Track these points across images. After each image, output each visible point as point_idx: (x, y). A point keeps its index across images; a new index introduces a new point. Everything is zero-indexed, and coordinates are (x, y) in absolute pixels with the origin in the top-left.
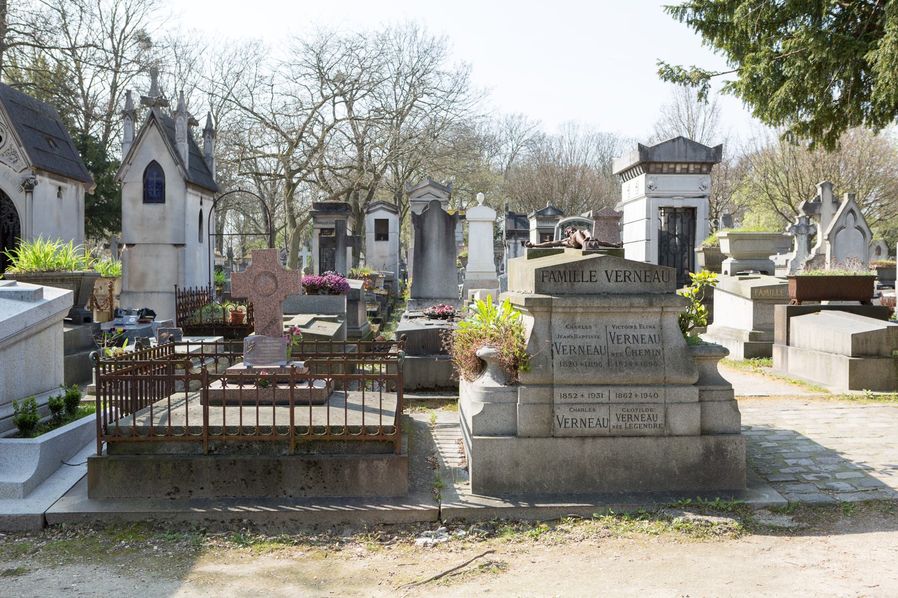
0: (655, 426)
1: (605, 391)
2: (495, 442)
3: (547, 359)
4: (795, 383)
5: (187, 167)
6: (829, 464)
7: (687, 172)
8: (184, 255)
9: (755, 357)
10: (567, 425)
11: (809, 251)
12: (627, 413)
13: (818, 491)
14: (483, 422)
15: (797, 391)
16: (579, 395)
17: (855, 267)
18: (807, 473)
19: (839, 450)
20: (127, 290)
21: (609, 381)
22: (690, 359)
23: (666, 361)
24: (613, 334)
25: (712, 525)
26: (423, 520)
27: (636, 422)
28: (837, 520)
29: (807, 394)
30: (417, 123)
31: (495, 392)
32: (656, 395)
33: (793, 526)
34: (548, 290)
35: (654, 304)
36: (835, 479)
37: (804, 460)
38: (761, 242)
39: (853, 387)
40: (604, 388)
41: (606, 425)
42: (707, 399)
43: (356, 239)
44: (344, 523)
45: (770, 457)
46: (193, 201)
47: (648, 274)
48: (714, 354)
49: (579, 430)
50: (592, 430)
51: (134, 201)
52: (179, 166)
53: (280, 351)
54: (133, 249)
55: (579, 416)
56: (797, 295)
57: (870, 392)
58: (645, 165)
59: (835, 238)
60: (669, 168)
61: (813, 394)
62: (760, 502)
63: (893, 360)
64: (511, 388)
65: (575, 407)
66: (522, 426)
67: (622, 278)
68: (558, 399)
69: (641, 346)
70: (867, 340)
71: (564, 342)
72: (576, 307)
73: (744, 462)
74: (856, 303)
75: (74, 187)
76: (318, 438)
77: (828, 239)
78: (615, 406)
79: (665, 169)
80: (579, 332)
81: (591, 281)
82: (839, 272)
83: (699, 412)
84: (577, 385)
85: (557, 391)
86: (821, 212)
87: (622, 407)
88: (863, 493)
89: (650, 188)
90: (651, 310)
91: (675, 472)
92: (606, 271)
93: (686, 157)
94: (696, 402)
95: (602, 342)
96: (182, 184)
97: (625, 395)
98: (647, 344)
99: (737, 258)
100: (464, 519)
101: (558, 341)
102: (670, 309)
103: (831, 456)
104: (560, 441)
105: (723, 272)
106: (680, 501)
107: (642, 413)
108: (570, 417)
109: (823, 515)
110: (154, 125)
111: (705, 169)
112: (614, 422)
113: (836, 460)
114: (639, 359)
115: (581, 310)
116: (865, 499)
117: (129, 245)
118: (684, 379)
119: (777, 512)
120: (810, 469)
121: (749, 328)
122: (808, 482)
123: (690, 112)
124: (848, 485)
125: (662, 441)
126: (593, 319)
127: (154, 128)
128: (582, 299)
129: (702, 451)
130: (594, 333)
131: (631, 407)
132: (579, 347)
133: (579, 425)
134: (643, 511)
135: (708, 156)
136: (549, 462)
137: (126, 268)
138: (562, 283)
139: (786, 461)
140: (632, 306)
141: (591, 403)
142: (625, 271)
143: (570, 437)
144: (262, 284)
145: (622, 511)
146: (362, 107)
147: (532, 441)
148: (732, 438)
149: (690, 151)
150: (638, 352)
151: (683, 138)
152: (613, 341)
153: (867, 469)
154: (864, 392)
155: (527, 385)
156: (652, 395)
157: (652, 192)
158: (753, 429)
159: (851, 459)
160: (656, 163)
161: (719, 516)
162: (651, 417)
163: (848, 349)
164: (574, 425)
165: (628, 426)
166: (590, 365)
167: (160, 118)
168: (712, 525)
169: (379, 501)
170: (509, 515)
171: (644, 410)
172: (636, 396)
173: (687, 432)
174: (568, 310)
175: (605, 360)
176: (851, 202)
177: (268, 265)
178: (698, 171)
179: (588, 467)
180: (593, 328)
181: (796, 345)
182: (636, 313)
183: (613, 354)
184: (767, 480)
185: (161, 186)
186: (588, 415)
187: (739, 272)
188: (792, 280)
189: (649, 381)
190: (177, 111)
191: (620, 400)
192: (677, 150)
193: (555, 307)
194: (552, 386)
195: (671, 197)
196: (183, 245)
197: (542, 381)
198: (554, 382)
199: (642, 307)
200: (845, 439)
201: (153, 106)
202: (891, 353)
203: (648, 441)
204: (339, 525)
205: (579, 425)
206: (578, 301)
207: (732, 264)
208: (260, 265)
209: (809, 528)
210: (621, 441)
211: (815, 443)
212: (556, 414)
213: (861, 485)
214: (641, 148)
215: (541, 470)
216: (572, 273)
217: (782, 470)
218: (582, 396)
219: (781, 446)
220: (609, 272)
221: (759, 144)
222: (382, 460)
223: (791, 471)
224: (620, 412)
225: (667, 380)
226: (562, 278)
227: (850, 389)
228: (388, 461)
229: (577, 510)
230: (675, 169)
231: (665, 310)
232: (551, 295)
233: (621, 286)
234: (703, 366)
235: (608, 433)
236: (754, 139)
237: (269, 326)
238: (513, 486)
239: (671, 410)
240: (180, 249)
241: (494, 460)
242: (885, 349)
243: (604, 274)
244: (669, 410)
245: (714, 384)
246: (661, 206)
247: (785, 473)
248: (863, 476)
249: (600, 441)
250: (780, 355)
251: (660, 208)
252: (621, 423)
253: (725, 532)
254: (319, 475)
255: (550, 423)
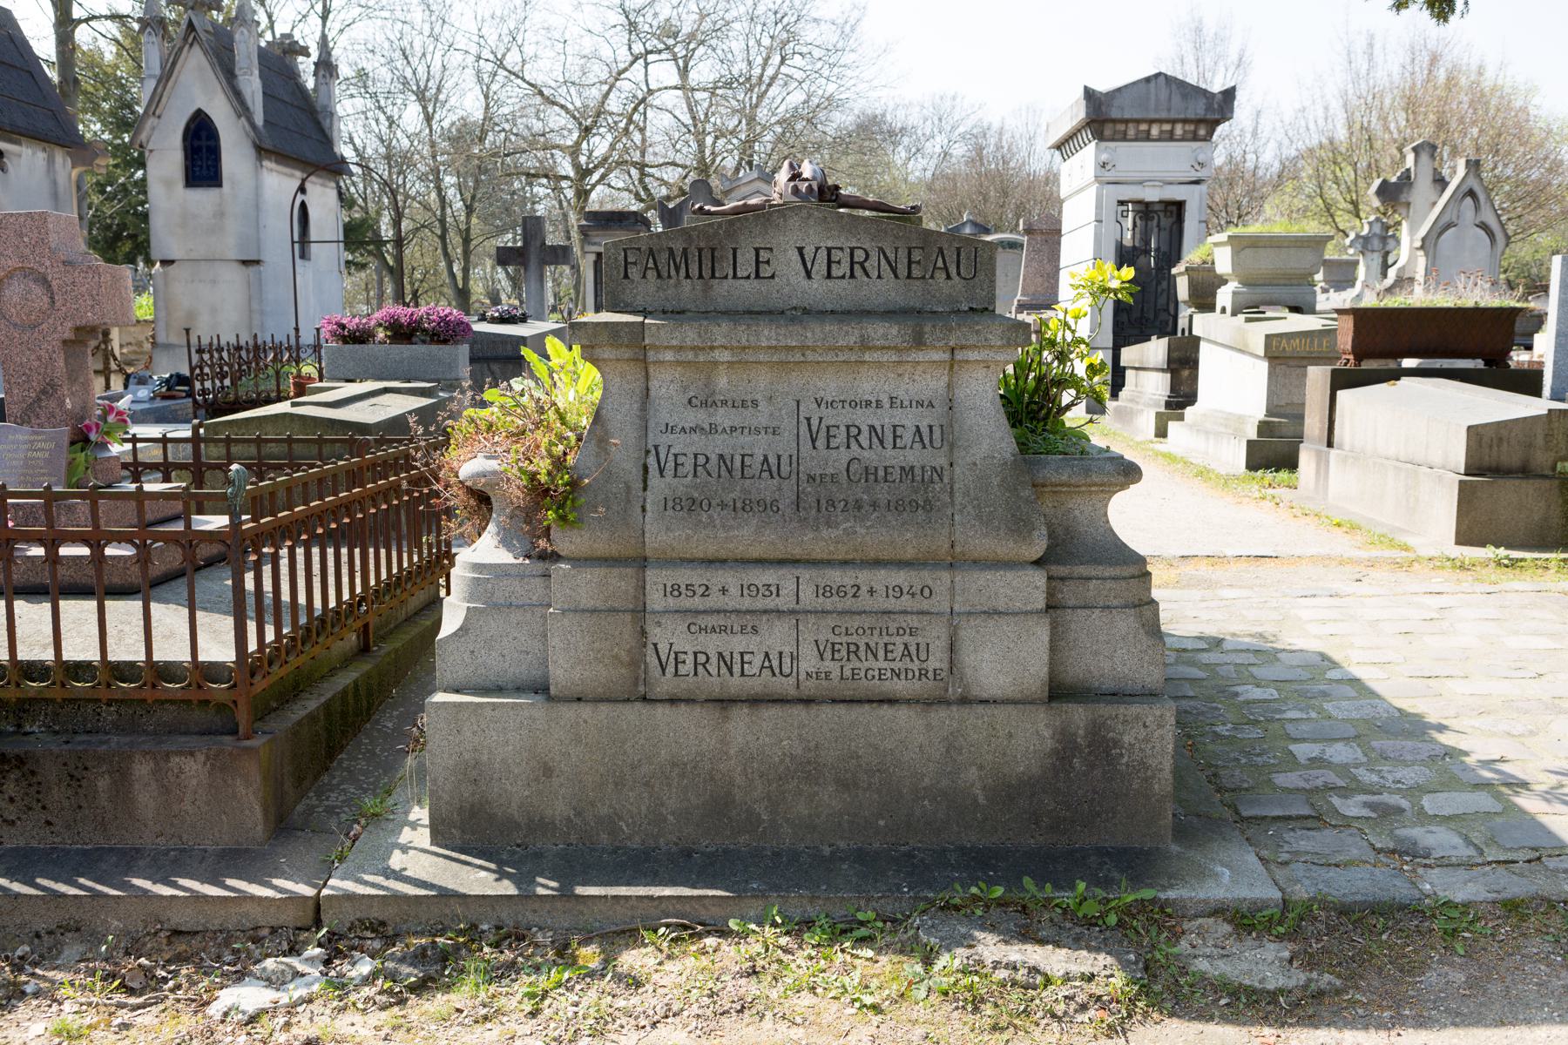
0: (923, 673)
1: (784, 579)
2: (488, 713)
3: (628, 489)
4: (1339, 525)
5: (259, 119)
6: (1405, 764)
7: (1171, 137)
8: (260, 280)
9: (1267, 467)
10: (683, 669)
11: (1385, 275)
12: (844, 639)
13: (1371, 856)
14: (466, 656)
15: (1342, 545)
16: (714, 589)
17: (1477, 291)
18: (1345, 792)
19: (1432, 718)
20: (165, 341)
21: (797, 552)
22: (1026, 492)
23: (958, 498)
24: (815, 422)
25: (1048, 981)
26: (274, 923)
27: (871, 663)
28: (1423, 967)
29: (1364, 554)
30: (784, 100)
31: (497, 577)
32: (927, 591)
33: (1291, 983)
34: (640, 302)
35: (928, 338)
36: (1423, 817)
37: (1339, 746)
38: (1292, 251)
39: (1463, 538)
40: (783, 571)
41: (786, 670)
42: (1071, 603)
43: (560, 252)
44: (65, 929)
45: (1255, 733)
46: (279, 183)
47: (916, 256)
48: (1095, 478)
49: (715, 681)
50: (749, 682)
51: (168, 184)
52: (243, 119)
53: (48, 461)
54: (171, 268)
55: (713, 644)
56: (1353, 347)
57: (1502, 552)
58: (1096, 125)
59: (1435, 245)
60: (1138, 131)
61: (1375, 553)
62: (1202, 895)
63: (1557, 482)
64: (540, 566)
65: (704, 621)
66: (561, 674)
67: (845, 268)
68: (656, 600)
69: (891, 457)
70: (1501, 439)
71: (679, 443)
72: (712, 348)
73: (1167, 774)
74: (1479, 364)
75: (41, 156)
76: (31, 694)
77: (1422, 247)
78: (812, 619)
79: (1131, 132)
80: (724, 417)
81: (758, 276)
82: (1443, 300)
83: (1046, 639)
84: (710, 562)
85: (656, 579)
86: (1411, 200)
87: (831, 621)
88: (1501, 869)
89: (1103, 167)
90: (920, 356)
91: (975, 800)
92: (800, 250)
93: (1169, 110)
94: (1038, 612)
95: (784, 445)
96: (250, 152)
97: (840, 591)
98: (908, 452)
99: (1244, 283)
100: (383, 924)
101: (664, 440)
102: (973, 355)
103: (1409, 735)
104: (661, 711)
105: (1218, 308)
106: (974, 890)
107: (886, 639)
108: (690, 649)
109: (1381, 945)
110: (196, 44)
111: (1202, 132)
112: (809, 663)
113: (1425, 750)
114: (882, 493)
115: (725, 356)
116: (1506, 895)
117: (166, 263)
118: (1006, 547)
119: (1250, 928)
120: (1354, 779)
121: (1260, 413)
122: (1346, 823)
123: (1201, 69)
124: (1457, 841)
125: (940, 715)
126: (762, 380)
127: (196, 49)
128: (725, 326)
129: (1050, 744)
130: (763, 420)
131: (855, 622)
132: (721, 456)
133: (713, 669)
134: (871, 915)
135: (1209, 108)
136: (633, 767)
137: (161, 304)
138: (678, 284)
139: (1292, 747)
140: (865, 345)
141: (748, 612)
142: (852, 250)
143: (690, 701)
144: (16, 299)
145: (811, 911)
146: (704, 71)
147: (586, 711)
148: (1135, 709)
149: (1176, 99)
150: (881, 473)
151: (1166, 75)
152: (813, 441)
153: (1508, 785)
154: (1489, 552)
155: (579, 561)
156: (915, 589)
157: (1107, 174)
158: (1226, 646)
159: (1463, 746)
160: (1114, 121)
161: (1077, 943)
162: (913, 649)
163: (1459, 458)
164: (700, 668)
165: (848, 673)
166: (746, 506)
167: (207, 31)
168: (1048, 981)
169: (167, 866)
170: (504, 915)
171: (892, 630)
172: (871, 591)
173: (1010, 692)
174: (690, 356)
175: (789, 495)
176: (1471, 175)
177: (27, 251)
178: (1190, 136)
179: (739, 780)
180: (762, 405)
181: (1347, 447)
182: (880, 364)
183: (811, 478)
184: (1237, 812)
185: (214, 152)
186: (737, 643)
187: (1250, 307)
188: (1345, 317)
189: (910, 553)
190: (236, 18)
191: (828, 604)
192: (1153, 97)
193: (654, 347)
194: (642, 562)
195: (1140, 183)
196: (257, 262)
197: (614, 550)
198: (649, 553)
199: (895, 348)
200: (1449, 682)
201: (192, 8)
202: (1554, 468)
203: (903, 714)
204: (50, 933)
205: (713, 669)
206: (716, 329)
207: (1234, 293)
208: (9, 252)
209: (1338, 992)
210: (827, 712)
211: (1373, 694)
212: (652, 639)
213: (1492, 841)
214: (1089, 94)
215: (611, 786)
216: (707, 255)
217: (1281, 780)
218: (724, 591)
219: (1285, 701)
220: (809, 252)
221: (1311, 117)
222: (192, 754)
223: (1302, 784)
224: (825, 635)
225: (958, 549)
226: (677, 269)
227: (1459, 542)
228: (208, 758)
229: (688, 908)
230: (1148, 132)
231: (959, 356)
232: (645, 313)
233: (841, 291)
234: (1070, 510)
235: (793, 692)
236: (1304, 110)
237: (39, 399)
238: (540, 826)
239: (966, 634)
240: (252, 269)
241: (485, 758)
242: (1541, 459)
243: (795, 257)
244: (962, 633)
245: (1096, 561)
246: (1122, 198)
247: (1285, 790)
248: (1499, 808)
249: (771, 713)
250: (1313, 465)
251: (1121, 203)
252: (828, 665)
253: (1083, 1008)
254: (33, 790)
255: (636, 662)
